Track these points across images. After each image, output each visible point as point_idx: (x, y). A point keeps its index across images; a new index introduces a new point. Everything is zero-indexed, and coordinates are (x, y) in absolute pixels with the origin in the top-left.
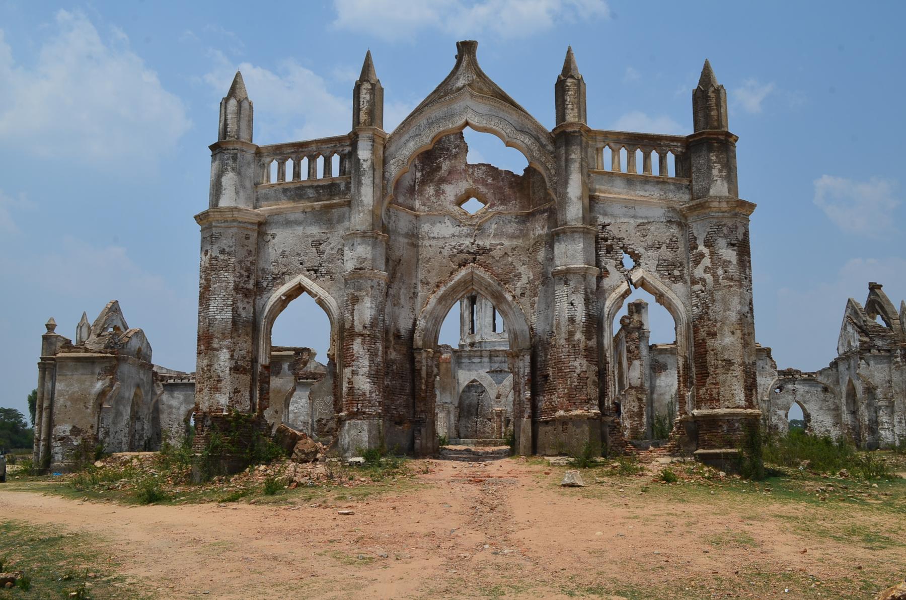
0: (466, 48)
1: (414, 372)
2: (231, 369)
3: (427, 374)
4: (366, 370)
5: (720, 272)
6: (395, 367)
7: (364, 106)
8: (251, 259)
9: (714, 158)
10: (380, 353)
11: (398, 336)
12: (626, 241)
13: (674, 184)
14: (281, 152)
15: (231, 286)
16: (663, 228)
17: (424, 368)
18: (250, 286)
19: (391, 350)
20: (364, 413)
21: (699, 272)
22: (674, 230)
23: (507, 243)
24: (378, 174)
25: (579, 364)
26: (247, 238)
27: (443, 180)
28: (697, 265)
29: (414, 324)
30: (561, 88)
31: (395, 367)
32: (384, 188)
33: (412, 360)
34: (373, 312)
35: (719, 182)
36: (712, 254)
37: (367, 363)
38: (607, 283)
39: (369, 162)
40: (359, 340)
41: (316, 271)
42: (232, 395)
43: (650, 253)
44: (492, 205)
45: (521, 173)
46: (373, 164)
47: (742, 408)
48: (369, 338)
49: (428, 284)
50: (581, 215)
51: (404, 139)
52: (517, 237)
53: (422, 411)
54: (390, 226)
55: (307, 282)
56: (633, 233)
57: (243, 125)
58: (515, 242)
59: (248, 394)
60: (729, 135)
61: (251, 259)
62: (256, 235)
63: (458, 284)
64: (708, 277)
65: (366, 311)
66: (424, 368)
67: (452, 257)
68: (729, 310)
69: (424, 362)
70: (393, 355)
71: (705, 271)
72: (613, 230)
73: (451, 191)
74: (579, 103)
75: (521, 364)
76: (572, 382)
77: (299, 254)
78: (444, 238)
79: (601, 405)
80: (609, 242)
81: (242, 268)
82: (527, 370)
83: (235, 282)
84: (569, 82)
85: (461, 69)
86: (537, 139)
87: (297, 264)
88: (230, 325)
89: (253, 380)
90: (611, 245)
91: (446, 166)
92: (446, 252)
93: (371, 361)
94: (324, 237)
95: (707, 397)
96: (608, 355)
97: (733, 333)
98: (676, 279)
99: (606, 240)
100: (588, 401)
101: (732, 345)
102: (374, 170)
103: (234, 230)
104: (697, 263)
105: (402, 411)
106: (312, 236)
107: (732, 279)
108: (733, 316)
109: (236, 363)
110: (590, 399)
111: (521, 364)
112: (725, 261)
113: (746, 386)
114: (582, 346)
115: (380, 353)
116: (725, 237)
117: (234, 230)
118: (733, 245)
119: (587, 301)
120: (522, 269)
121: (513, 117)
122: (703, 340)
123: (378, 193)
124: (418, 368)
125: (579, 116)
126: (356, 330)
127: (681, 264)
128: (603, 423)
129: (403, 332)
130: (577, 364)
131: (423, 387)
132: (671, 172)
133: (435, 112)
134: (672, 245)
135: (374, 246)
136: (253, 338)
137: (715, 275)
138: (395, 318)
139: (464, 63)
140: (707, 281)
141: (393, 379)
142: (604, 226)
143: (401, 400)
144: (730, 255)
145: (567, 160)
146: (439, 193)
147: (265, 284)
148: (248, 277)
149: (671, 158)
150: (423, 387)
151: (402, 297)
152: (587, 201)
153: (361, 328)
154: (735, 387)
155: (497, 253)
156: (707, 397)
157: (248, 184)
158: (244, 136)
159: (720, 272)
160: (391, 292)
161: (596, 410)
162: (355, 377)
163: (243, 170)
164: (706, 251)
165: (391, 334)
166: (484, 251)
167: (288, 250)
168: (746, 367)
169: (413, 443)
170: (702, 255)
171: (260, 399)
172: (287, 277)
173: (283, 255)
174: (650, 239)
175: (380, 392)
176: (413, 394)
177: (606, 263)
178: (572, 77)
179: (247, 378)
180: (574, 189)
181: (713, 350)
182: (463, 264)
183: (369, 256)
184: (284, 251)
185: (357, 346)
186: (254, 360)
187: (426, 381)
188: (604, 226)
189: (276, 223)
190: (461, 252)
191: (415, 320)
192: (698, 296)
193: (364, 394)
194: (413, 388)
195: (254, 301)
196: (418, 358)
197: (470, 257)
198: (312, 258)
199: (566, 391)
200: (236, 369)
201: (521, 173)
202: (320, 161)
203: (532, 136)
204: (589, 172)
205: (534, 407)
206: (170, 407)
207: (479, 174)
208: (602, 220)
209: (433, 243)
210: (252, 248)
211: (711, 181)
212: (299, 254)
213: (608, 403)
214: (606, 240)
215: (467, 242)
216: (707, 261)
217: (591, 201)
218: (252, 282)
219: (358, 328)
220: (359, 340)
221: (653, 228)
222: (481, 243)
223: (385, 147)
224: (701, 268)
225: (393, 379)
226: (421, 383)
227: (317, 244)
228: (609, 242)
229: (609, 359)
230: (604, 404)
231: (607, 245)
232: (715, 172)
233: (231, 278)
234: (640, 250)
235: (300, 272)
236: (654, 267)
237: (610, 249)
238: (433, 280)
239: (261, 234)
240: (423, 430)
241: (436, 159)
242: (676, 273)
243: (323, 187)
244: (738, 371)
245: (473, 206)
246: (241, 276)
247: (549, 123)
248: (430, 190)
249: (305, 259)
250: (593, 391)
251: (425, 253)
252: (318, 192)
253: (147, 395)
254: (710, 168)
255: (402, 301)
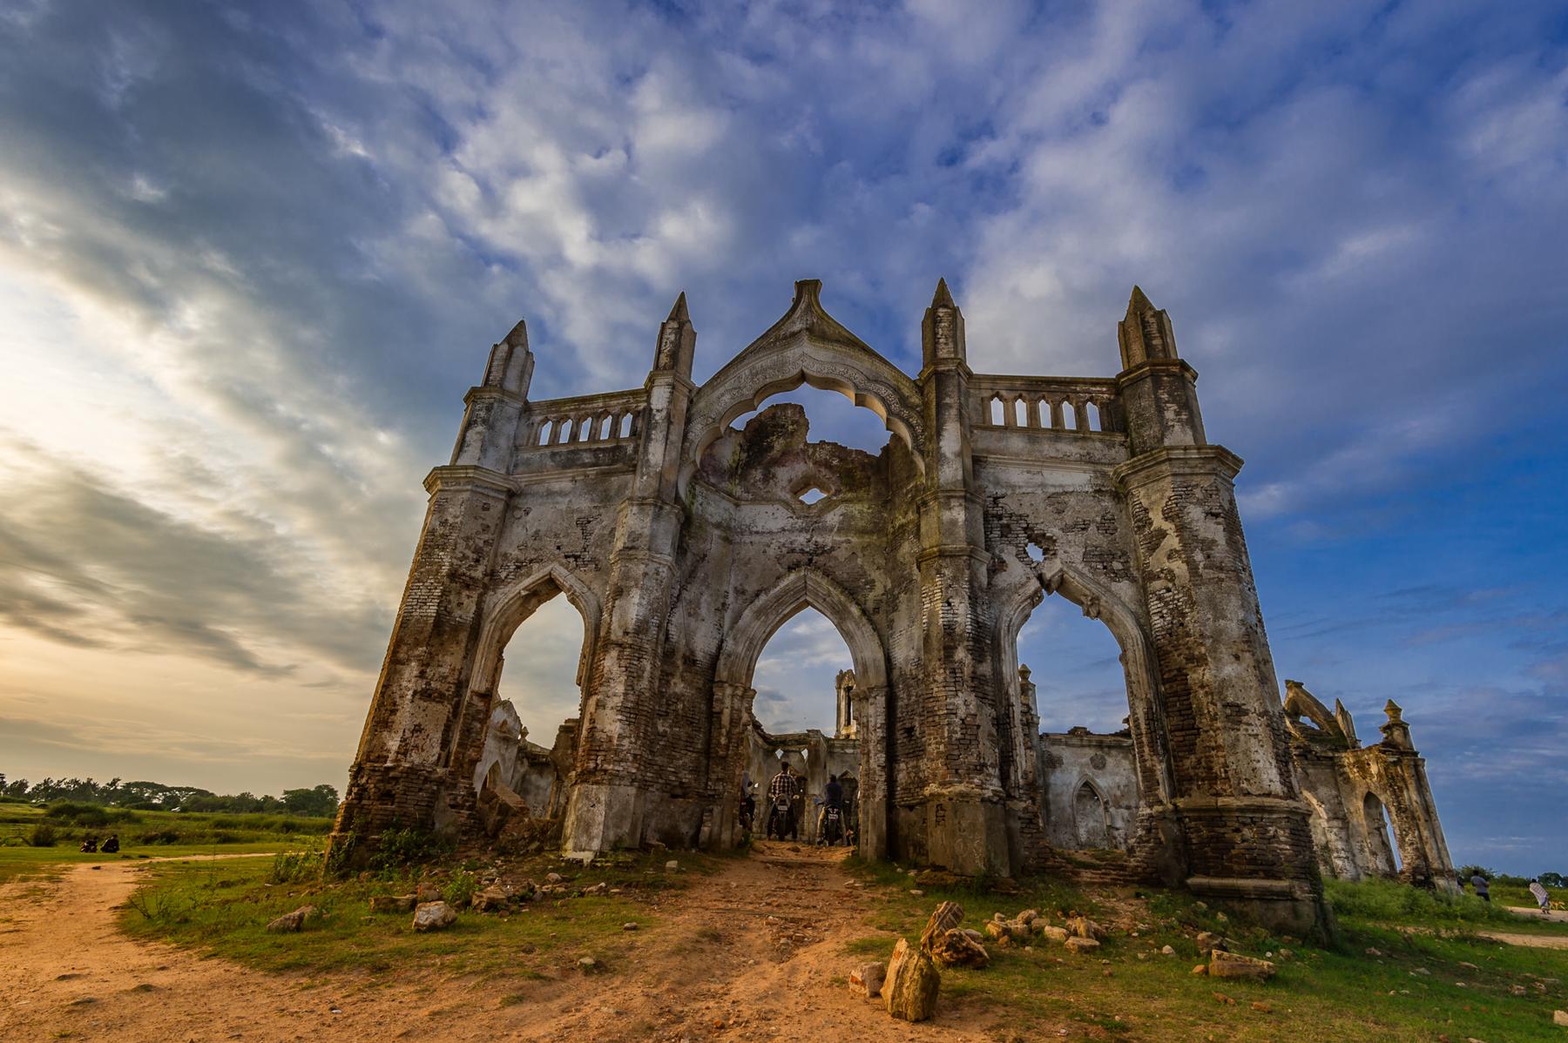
0: (807, 288)
1: (713, 716)
2: (415, 693)
3: (731, 721)
4: (617, 701)
5: (1199, 556)
6: (680, 706)
7: (667, 348)
8: (486, 537)
9: (1165, 396)
10: (646, 675)
11: (690, 660)
12: (1031, 520)
13: (1101, 441)
14: (558, 410)
15: (445, 570)
16: (1090, 501)
17: (727, 712)
18: (478, 573)
19: (676, 680)
20: (606, 771)
21: (1158, 561)
22: (1107, 503)
23: (854, 540)
24: (675, 437)
25: (964, 702)
26: (486, 508)
27: (777, 462)
28: (1154, 550)
29: (720, 648)
30: (932, 319)
31: (680, 706)
32: (683, 451)
33: (709, 698)
34: (642, 611)
35: (1177, 428)
36: (1181, 529)
37: (620, 689)
38: (1002, 580)
39: (664, 413)
40: (614, 653)
41: (576, 558)
42: (408, 734)
43: (1071, 536)
44: (838, 492)
45: (878, 453)
46: (668, 417)
47: (1276, 796)
48: (632, 650)
49: (743, 592)
50: (960, 477)
51: (717, 393)
52: (871, 533)
53: (718, 780)
54: (694, 508)
55: (560, 572)
56: (1041, 509)
57: (513, 373)
58: (867, 539)
59: (439, 735)
60: (1184, 366)
61: (486, 537)
62: (500, 506)
63: (786, 592)
64: (1179, 567)
65: (634, 608)
66: (727, 712)
67: (778, 559)
68: (1224, 617)
69: (728, 702)
70: (678, 686)
71: (1169, 557)
72: (1010, 504)
73: (784, 474)
74: (954, 337)
75: (871, 710)
76: (952, 732)
77: (556, 536)
78: (771, 533)
79: (1004, 778)
80: (1005, 521)
81: (468, 547)
82: (881, 720)
83: (452, 564)
84: (942, 312)
85: (798, 312)
86: (897, 390)
87: (552, 547)
88: (429, 628)
89: (455, 713)
90: (1008, 526)
91: (778, 445)
92: (772, 552)
93: (630, 687)
94: (595, 512)
95: (1202, 772)
96: (1011, 691)
97: (1237, 658)
98: (1117, 576)
99: (1000, 517)
100: (980, 768)
101: (1239, 677)
102: (670, 423)
103: (466, 495)
104: (1153, 549)
105: (687, 777)
106: (579, 511)
107: (1221, 569)
108: (1233, 628)
109: (428, 684)
110: (984, 765)
111: (871, 710)
112: (1203, 541)
113: (1277, 755)
114: (967, 671)
115: (646, 675)
116: (1199, 503)
117: (466, 495)
118: (1217, 515)
119: (974, 601)
120: (875, 575)
121: (866, 364)
122: (1179, 670)
123: (674, 454)
124: (716, 709)
125: (956, 352)
126: (613, 637)
127: (1124, 554)
128: (1009, 813)
129: (700, 656)
130: (959, 701)
131: (723, 741)
132: (1094, 424)
133: (765, 361)
134: (1107, 525)
135: (657, 517)
136: (467, 650)
137: (1191, 564)
138: (689, 635)
139: (802, 306)
140: (1177, 571)
141: (675, 724)
142: (996, 499)
143: (686, 759)
144: (1215, 531)
145: (940, 407)
146: (768, 477)
147: (503, 575)
148: (477, 561)
149: (1092, 410)
150: (723, 741)
151: (704, 606)
152: (969, 462)
153: (620, 633)
154: (1258, 757)
155: (841, 554)
156: (1202, 772)
157: (503, 442)
158: (511, 385)
159: (1199, 556)
160: (685, 595)
161: (995, 785)
162: (600, 711)
163: (498, 424)
164: (1168, 526)
165: (679, 656)
166: (820, 550)
167: (543, 529)
168: (1271, 718)
169: (698, 830)
170: (1162, 534)
171: (460, 745)
172: (536, 566)
173: (536, 535)
174: (1069, 517)
175: (638, 737)
176: (708, 752)
177: (1002, 551)
178: (945, 306)
179: (443, 710)
180: (950, 441)
181: (1202, 687)
182: (791, 568)
183: (647, 531)
184: (537, 532)
185: (610, 662)
186: (461, 685)
187: (729, 733)
188: (996, 499)
189: (533, 495)
190: (793, 551)
191: (722, 641)
192: (1160, 599)
193: (610, 739)
194: (708, 742)
195: (481, 596)
196: (718, 694)
197: (805, 558)
198: (574, 542)
199: (942, 747)
200: (425, 694)
201: (878, 453)
202: (566, 428)
203: (889, 386)
204: (975, 424)
205: (891, 782)
206: (538, 788)
207: (821, 455)
208: (992, 490)
209: (756, 538)
210: (491, 522)
211: (1165, 428)
212: (556, 536)
213: (1017, 777)
214: (1000, 517)
215: (801, 539)
216: (1172, 541)
217: (977, 462)
218: (481, 568)
219: (616, 634)
220: (614, 653)
221: (1072, 500)
222: (820, 540)
223: (691, 401)
224: (1161, 553)
225: (675, 724)
226: (720, 734)
227: (584, 523)
228: (1005, 521)
229: (1013, 700)
230: (1008, 777)
231: (1002, 526)
232: (1169, 415)
233: (447, 560)
234: (1053, 531)
235: (555, 559)
236: (1079, 557)
237: (1006, 530)
238: (751, 588)
239: (509, 507)
240: (717, 810)
241: (767, 442)
242: (1117, 565)
243: (604, 450)
244: (1258, 726)
245: (813, 496)
246: (465, 557)
247: (913, 368)
248: (757, 474)
249: (565, 541)
250: (991, 756)
251: (747, 552)
252: (596, 457)
253: (506, 771)
254: (1160, 411)
255: (703, 611)
